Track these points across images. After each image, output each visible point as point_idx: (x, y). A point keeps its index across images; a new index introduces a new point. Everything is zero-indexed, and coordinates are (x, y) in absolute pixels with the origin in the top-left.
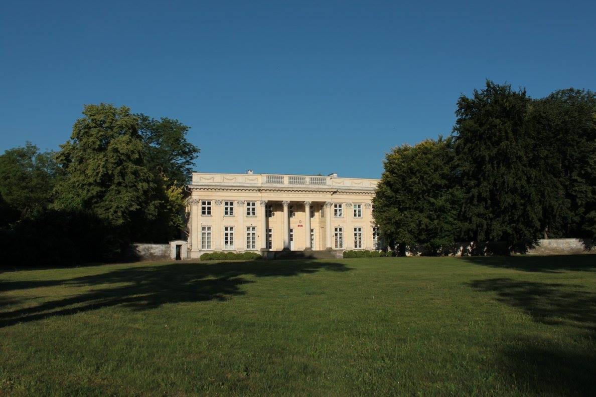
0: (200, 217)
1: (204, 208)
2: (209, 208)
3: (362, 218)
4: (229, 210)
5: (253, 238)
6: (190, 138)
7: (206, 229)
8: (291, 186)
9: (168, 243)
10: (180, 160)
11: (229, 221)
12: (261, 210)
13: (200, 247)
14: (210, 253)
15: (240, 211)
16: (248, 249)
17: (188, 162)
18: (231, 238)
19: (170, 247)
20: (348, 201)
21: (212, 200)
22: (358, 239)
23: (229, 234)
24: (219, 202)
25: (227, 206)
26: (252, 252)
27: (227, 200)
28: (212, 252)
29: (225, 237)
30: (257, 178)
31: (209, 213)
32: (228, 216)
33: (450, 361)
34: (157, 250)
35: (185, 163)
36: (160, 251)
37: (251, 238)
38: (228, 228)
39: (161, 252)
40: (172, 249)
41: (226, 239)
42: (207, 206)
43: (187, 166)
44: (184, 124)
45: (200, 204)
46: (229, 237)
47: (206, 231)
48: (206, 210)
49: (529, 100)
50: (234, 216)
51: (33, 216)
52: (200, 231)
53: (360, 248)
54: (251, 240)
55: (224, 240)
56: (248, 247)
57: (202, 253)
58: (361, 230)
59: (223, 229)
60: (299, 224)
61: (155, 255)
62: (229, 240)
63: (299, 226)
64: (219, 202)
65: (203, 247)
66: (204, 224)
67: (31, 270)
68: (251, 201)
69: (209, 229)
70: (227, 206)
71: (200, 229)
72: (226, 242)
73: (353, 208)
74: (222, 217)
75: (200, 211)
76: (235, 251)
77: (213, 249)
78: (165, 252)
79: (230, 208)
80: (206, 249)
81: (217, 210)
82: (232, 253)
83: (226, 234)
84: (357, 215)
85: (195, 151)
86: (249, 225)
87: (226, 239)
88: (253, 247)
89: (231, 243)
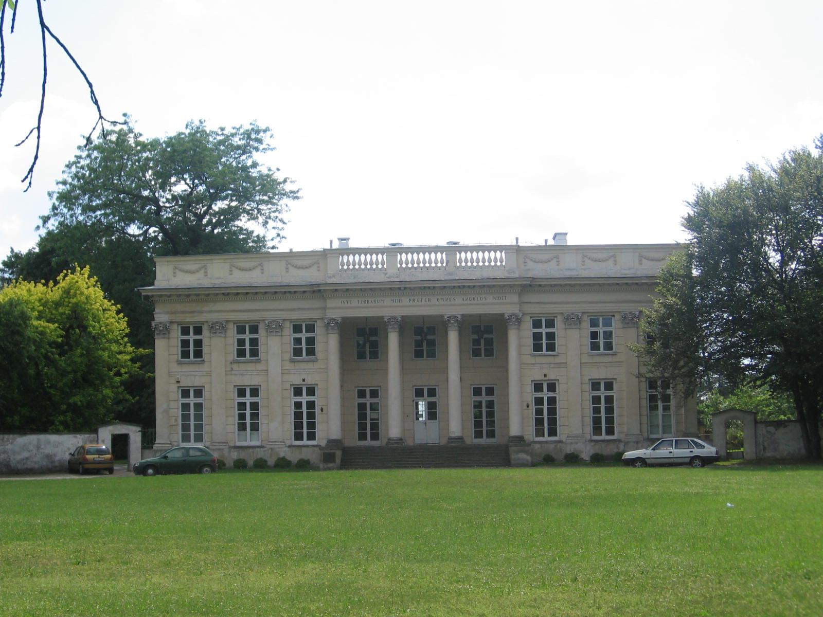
1: (185, 343)
2: (551, 336)
4: (248, 350)
5: (311, 415)
11: (248, 375)
12: (329, 346)
15: (275, 347)
18: (255, 416)
20: (568, 309)
21: (203, 323)
22: (603, 414)
24: (573, 320)
25: (298, 335)
29: (237, 412)
30: (205, 266)
32: (424, 363)
38: (599, 384)
46: (248, 412)
47: (192, 400)
48: (192, 351)
53: (375, 443)
54: (192, 423)
62: (248, 421)
64: (573, 320)
66: (186, 383)
67: (798, 469)
68: (304, 320)
71: (176, 395)
72: (242, 427)
73: (587, 329)
79: (605, 333)
81: (219, 349)
86: (297, 381)
89: (255, 428)
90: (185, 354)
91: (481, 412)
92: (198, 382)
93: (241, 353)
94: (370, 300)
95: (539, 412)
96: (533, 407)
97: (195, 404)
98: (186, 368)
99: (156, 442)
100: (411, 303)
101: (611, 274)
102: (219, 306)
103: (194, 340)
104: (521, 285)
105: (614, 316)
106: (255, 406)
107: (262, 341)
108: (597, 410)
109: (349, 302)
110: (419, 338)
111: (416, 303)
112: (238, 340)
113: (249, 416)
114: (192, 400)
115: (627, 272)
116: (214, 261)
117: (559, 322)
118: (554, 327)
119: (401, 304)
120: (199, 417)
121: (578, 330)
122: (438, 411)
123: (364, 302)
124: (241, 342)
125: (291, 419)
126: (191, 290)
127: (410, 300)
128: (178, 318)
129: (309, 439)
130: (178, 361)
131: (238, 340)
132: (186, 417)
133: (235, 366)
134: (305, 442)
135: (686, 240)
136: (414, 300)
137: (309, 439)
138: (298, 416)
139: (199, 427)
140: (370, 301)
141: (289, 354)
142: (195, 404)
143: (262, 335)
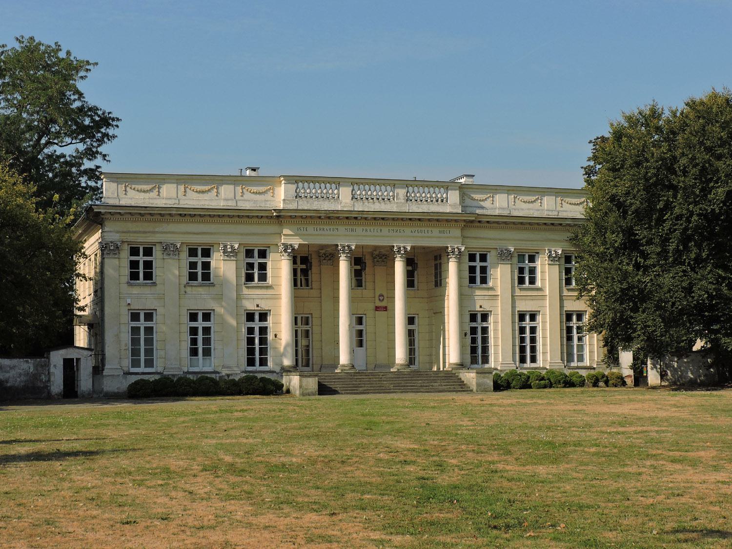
0: (125, 288)
1: (134, 265)
3: (492, 289)
6: (93, 91)
7: (142, 317)
8: (359, 207)
9: (41, 355)
10: (69, 148)
11: (200, 298)
12: (280, 269)
13: (126, 363)
14: (152, 378)
16: (250, 368)
17: (91, 154)
18: (207, 341)
19: (47, 365)
23: (200, 331)
25: (193, 259)
26: (259, 376)
27: (145, 285)
28: (157, 377)
29: (212, 336)
31: (148, 276)
33: (394, 486)
34: (12, 373)
35: (81, 156)
36: (20, 374)
37: (257, 341)
38: (196, 314)
39: (23, 378)
40: (52, 370)
41: (194, 342)
42: (141, 259)
43: (87, 164)
44: (78, 55)
45: (125, 253)
46: (200, 337)
47: (142, 324)
49: (50, 354)
50: (213, 285)
51: (260, 387)
52: (126, 324)
55: (186, 345)
56: (251, 362)
57: (133, 379)
58: (416, 320)
59: (186, 318)
60: (379, 304)
61: (9, 385)
62: (200, 346)
63: (377, 308)
65: (136, 363)
66: (136, 306)
69: (149, 316)
70: (193, 259)
71: (126, 317)
72: (194, 352)
74: (182, 286)
75: (126, 271)
76: (215, 372)
77: (160, 370)
78: (35, 376)
80: (142, 369)
82: (207, 378)
83: (194, 331)
84: (478, 279)
85: (106, 121)
87: (194, 342)
88: (263, 362)
89: (207, 352)
90: (134, 276)
91: (261, 354)
92: (149, 305)
93: (193, 277)
94: (325, 228)
95: (474, 340)
96: (469, 337)
97: (145, 328)
98: (135, 291)
99: (106, 367)
100: (364, 233)
101: (536, 214)
102: (172, 227)
103: (144, 261)
104: (465, 221)
105: (269, 247)
106: (207, 330)
107: (213, 264)
108: (522, 340)
109: (305, 229)
110: (358, 267)
111: (369, 233)
112: (470, 267)
113: (200, 339)
114: (142, 324)
115: (550, 213)
116: (452, 203)
117: (157, 252)
118: (151, 255)
119: (354, 233)
120: (149, 341)
121: (118, 260)
122: (355, 339)
123: (330, 230)
124: (193, 265)
125: (244, 344)
126: (148, 209)
127: (363, 230)
128: (131, 238)
129: (261, 365)
130: (128, 283)
131: (470, 267)
132: (135, 342)
133: (189, 289)
134: (257, 367)
135: (117, 126)
136: (330, 230)
137: (261, 365)
138: (250, 341)
139: (149, 352)
140: (368, 230)
141: (185, 279)
142: (145, 328)
143: (157, 257)
